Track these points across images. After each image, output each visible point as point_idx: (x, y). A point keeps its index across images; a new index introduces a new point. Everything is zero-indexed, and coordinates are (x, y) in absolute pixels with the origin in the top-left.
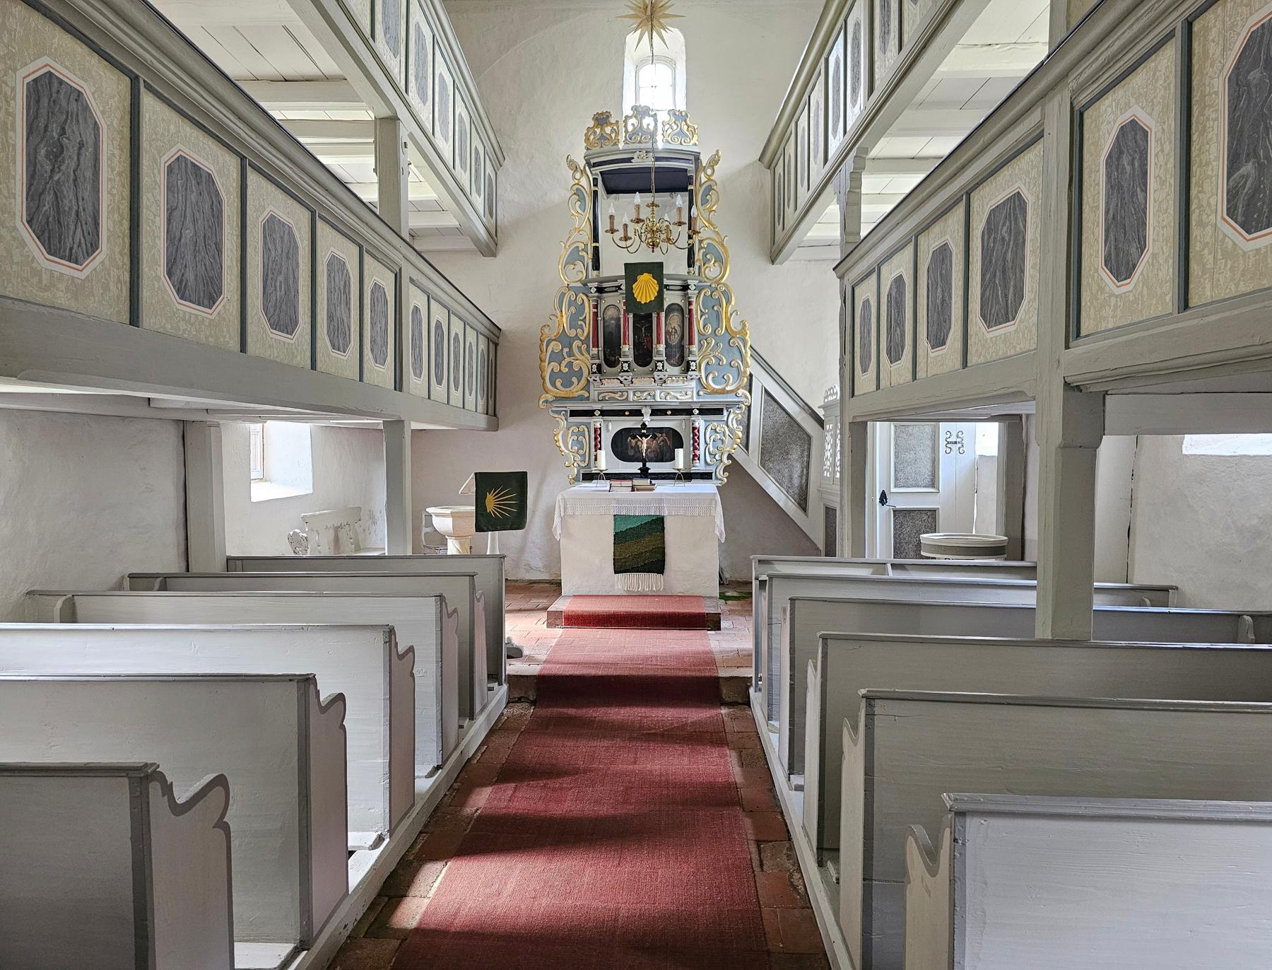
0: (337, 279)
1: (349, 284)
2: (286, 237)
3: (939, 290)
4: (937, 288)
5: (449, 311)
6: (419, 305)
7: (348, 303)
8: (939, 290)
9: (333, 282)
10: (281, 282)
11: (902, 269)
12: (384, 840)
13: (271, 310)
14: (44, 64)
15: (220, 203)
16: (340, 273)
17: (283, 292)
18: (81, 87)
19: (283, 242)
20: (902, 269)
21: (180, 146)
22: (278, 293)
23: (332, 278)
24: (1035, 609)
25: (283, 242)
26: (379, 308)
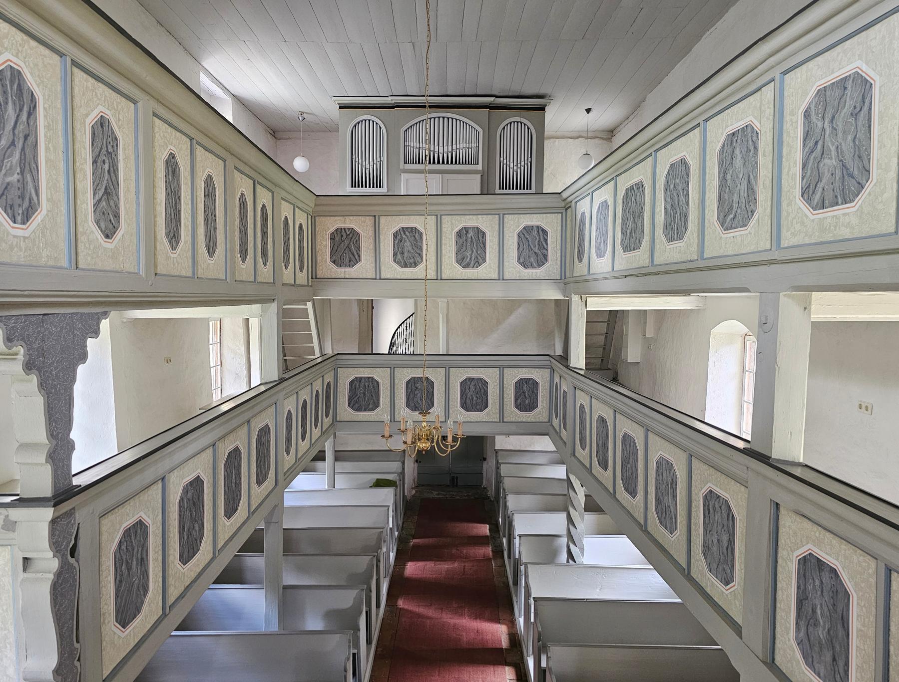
0: (665, 475)
1: (676, 482)
2: (632, 444)
3: (234, 477)
4: (232, 476)
5: (254, 182)
6: (584, 403)
7: (675, 496)
8: (234, 477)
9: (661, 476)
10: (629, 468)
11: (199, 471)
12: (513, 585)
13: (625, 481)
14: (808, 549)
15: (608, 430)
16: (668, 472)
17: (630, 474)
18: (836, 566)
19: (630, 446)
20: (199, 471)
21: (661, 452)
22: (628, 473)
23: (660, 474)
24: (263, 530)
25: (630, 446)
26: (556, 400)
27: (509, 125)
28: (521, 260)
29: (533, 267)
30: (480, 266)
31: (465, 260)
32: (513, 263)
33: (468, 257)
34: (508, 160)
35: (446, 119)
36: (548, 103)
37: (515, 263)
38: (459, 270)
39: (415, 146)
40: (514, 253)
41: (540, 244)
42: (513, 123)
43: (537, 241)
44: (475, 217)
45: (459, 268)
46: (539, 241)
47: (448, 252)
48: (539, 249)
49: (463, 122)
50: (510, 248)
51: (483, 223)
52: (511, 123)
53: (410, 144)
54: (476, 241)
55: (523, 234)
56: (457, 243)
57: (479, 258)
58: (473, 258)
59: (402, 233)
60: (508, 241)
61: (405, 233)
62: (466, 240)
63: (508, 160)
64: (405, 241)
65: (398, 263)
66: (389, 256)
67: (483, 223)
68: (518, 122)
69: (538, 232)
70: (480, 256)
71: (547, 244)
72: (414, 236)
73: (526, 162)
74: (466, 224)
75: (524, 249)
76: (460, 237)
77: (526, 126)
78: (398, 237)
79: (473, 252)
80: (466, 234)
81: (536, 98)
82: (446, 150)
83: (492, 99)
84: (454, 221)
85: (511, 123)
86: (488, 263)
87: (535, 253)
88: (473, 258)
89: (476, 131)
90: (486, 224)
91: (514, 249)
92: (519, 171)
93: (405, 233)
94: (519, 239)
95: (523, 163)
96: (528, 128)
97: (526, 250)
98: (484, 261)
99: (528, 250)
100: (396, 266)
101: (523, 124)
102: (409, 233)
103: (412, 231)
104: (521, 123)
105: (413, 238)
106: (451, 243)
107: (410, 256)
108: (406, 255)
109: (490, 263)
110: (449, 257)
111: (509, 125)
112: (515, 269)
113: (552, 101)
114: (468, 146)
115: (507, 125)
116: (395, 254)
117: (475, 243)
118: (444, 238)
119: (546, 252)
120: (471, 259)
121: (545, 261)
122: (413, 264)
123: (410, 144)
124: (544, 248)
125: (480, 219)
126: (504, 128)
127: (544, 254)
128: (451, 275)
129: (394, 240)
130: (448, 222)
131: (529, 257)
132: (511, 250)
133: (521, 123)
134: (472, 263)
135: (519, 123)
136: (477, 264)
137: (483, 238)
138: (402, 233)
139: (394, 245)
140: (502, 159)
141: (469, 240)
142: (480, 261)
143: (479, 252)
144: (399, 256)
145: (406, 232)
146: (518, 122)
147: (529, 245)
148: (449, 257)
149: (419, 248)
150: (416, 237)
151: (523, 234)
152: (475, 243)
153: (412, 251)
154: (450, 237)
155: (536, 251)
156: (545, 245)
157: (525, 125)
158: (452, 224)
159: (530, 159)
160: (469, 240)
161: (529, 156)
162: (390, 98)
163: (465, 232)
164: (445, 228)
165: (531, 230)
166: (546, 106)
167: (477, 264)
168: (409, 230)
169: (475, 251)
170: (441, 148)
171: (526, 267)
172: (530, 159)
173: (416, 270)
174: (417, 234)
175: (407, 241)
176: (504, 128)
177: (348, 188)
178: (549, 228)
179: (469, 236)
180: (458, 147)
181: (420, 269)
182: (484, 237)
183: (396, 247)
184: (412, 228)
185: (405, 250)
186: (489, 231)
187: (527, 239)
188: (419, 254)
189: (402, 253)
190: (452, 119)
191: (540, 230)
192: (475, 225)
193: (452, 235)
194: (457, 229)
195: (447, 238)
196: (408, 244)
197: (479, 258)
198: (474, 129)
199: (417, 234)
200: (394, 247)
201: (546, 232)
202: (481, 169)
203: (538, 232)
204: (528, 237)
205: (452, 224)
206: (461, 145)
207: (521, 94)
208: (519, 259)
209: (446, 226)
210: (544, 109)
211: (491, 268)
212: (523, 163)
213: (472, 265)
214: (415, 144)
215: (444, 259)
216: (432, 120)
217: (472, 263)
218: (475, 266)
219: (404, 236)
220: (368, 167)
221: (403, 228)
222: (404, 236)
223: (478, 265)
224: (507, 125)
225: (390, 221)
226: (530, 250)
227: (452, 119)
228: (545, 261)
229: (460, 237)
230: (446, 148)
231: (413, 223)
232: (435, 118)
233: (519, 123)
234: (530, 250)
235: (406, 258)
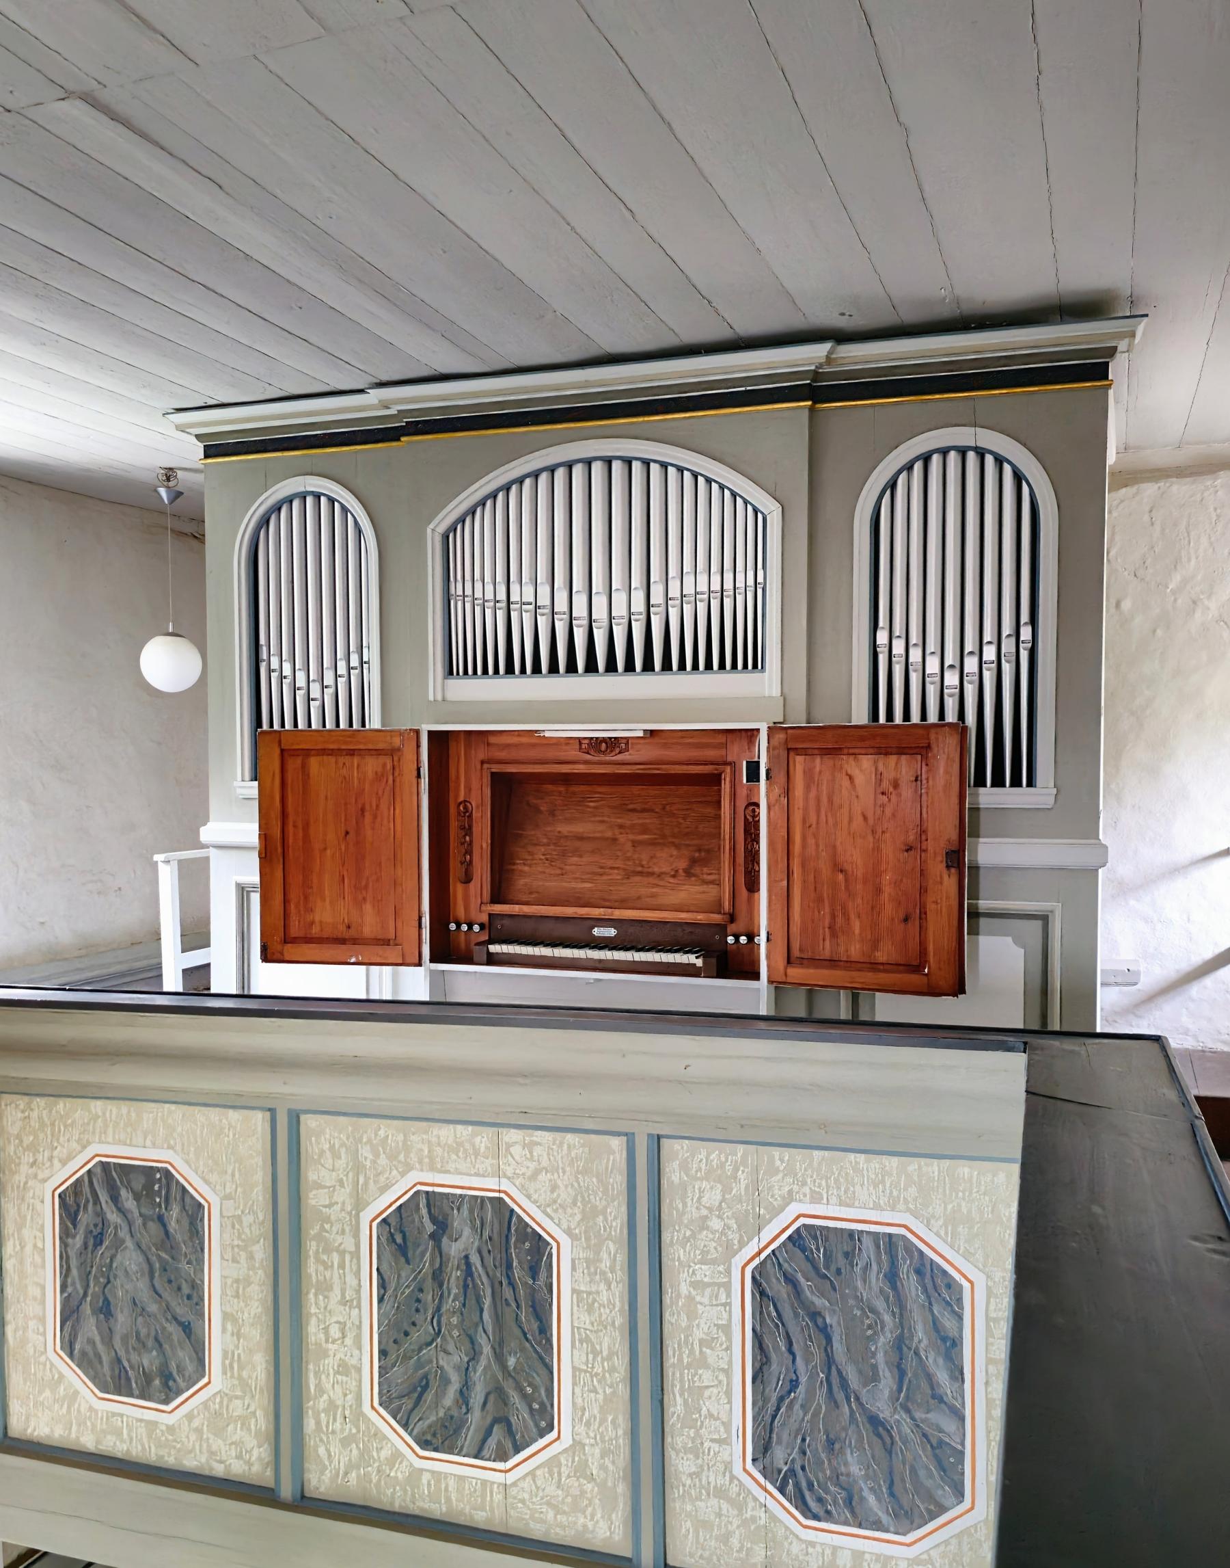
27: (918, 467)
28: (779, 1455)
29: (860, 1519)
30: (517, 1450)
31: (429, 1396)
32: (728, 1466)
33: (446, 1381)
34: (915, 637)
35: (617, 466)
36: (1121, 336)
37: (737, 1469)
38: (397, 1456)
39: (489, 595)
40: (729, 1393)
41: (910, 1364)
42: (936, 459)
43: (884, 1340)
44: (483, 1139)
45: (397, 1439)
46: (900, 1344)
47: (335, 1332)
48: (904, 1400)
49: (695, 476)
50: (703, 1363)
51: (534, 1177)
52: (926, 459)
53: (468, 592)
54: (496, 1287)
55: (790, 1280)
56: (383, 1285)
57: (515, 1397)
58: (477, 1396)
59: (103, 1197)
60: (692, 1315)
61: (115, 1198)
62: (438, 1276)
63: (915, 637)
64: (118, 1244)
65: (86, 1362)
66: (42, 1320)
67: (534, 1177)
68: (963, 452)
69: (892, 1277)
70: (521, 1390)
71: (957, 1374)
72: (160, 1219)
73: (1008, 646)
74: (440, 1178)
75: (794, 1384)
76: (405, 1254)
77: (1007, 469)
78: (85, 1218)
79: (474, 1355)
80: (433, 1236)
81: (1062, 322)
82: (619, 610)
83: (819, 351)
84: (366, 1153)
85: (926, 459)
86: (566, 1441)
87: (875, 1421)
88: (477, 1396)
89: (756, 511)
90: (554, 1188)
91: (728, 1372)
92: (1007, 668)
93: (115, 1198)
94: (759, 1311)
95: (990, 653)
96: (1018, 478)
97: (810, 1393)
98: (544, 1421)
99: (821, 1396)
100: (74, 1378)
101: (989, 459)
102: (137, 1197)
103: (148, 1186)
104: (981, 453)
105: (153, 1226)
106: (351, 1280)
107: (143, 1331)
108: (122, 1320)
109: (577, 1445)
110: (343, 1369)
111: (918, 467)
112: (740, 1508)
113: (1141, 327)
114: (716, 586)
115: (909, 467)
116: (70, 1314)
117: (487, 1303)
118: (312, 1247)
119: (949, 1425)
120: (464, 1395)
121: (944, 1493)
122: (157, 1382)
123: (468, 592)
124: (941, 1400)
125: (517, 1151)
126: (892, 485)
127: (934, 1436)
128: (353, 1475)
129: (65, 1235)
130: (336, 1156)
131: (830, 1443)
132: (707, 1377)
133: (981, 453)
134: (476, 1419)
135: (971, 456)
136: (498, 1432)
137: (534, 1271)
138: (103, 1197)
139: (64, 1257)
140: (882, 638)
141: (454, 1276)
142: (520, 1415)
143: (511, 1362)
144: (90, 1327)
145: (123, 1192)
146: (963, 452)
147: (829, 1361)
148: (344, 1368)
149: (186, 1290)
150: (173, 1226)
151: (790, 1280)
152: (487, 1303)
153: (153, 1308)
154: (349, 1244)
155: (882, 1405)
156: (942, 1377)
157: (1000, 461)
158: (358, 1168)
159: (1026, 633)
160: (454, 1276)
161: (1025, 616)
162: (374, 396)
163: (430, 1228)
164: (319, 1186)
165: (841, 1262)
166: (1112, 351)
167: (498, 1432)
168: (138, 1182)
169: (487, 1350)
170: (600, 603)
171: (812, 1504)
172: (1026, 633)
173: (171, 1420)
174: (175, 1211)
175: (129, 1243)
176: (892, 485)
177: (238, 783)
178: (967, 1256)
179: (454, 1249)
180: (674, 591)
181: (190, 1417)
182: (543, 1275)
183: (74, 1272)
184: (149, 1172)
185: (121, 1291)
186: (568, 1232)
187: (815, 1315)
188: (187, 1329)
189: (105, 1310)
190: (647, 463)
191: (904, 1269)
192: (485, 1184)
193: (356, 1235)
194: (384, 1203)
195: (328, 1251)
196: (130, 1259)
197: (515, 1397)
198: (746, 502)
199: (175, 1211)
200: (66, 1273)
201: (951, 1284)
202: (776, 692)
203: (892, 1277)
204: (820, 1302)
205: (358, 1168)
206: (689, 580)
207: (967, 309)
208: (763, 1448)
209: (328, 1179)
210: (1098, 372)
211: (581, 1471)
212: (990, 653)
213: (470, 1436)
214: (489, 588)
215: (317, 1374)
216: (560, 474)
217: (476, 1419)
218: (492, 1443)
219: (113, 1217)
220: (315, 691)
221: (105, 1166)
222: (113, 1217)
223: (509, 1445)
224: (909, 467)
225: (43, 1125)
226: (840, 1396)
227: (647, 463)
228: (944, 1493)
229: (405, 1254)
230: (619, 599)
231: (154, 1145)
232: (570, 466)
233: (971, 456)
234: (840, 1396)
235: (125, 1339)
